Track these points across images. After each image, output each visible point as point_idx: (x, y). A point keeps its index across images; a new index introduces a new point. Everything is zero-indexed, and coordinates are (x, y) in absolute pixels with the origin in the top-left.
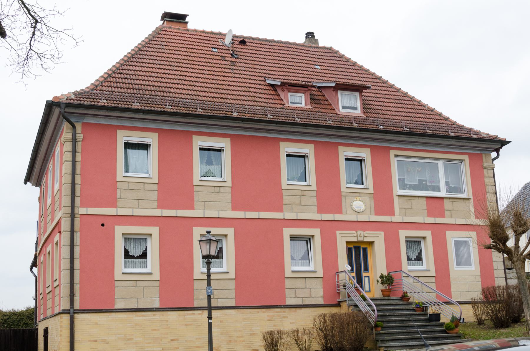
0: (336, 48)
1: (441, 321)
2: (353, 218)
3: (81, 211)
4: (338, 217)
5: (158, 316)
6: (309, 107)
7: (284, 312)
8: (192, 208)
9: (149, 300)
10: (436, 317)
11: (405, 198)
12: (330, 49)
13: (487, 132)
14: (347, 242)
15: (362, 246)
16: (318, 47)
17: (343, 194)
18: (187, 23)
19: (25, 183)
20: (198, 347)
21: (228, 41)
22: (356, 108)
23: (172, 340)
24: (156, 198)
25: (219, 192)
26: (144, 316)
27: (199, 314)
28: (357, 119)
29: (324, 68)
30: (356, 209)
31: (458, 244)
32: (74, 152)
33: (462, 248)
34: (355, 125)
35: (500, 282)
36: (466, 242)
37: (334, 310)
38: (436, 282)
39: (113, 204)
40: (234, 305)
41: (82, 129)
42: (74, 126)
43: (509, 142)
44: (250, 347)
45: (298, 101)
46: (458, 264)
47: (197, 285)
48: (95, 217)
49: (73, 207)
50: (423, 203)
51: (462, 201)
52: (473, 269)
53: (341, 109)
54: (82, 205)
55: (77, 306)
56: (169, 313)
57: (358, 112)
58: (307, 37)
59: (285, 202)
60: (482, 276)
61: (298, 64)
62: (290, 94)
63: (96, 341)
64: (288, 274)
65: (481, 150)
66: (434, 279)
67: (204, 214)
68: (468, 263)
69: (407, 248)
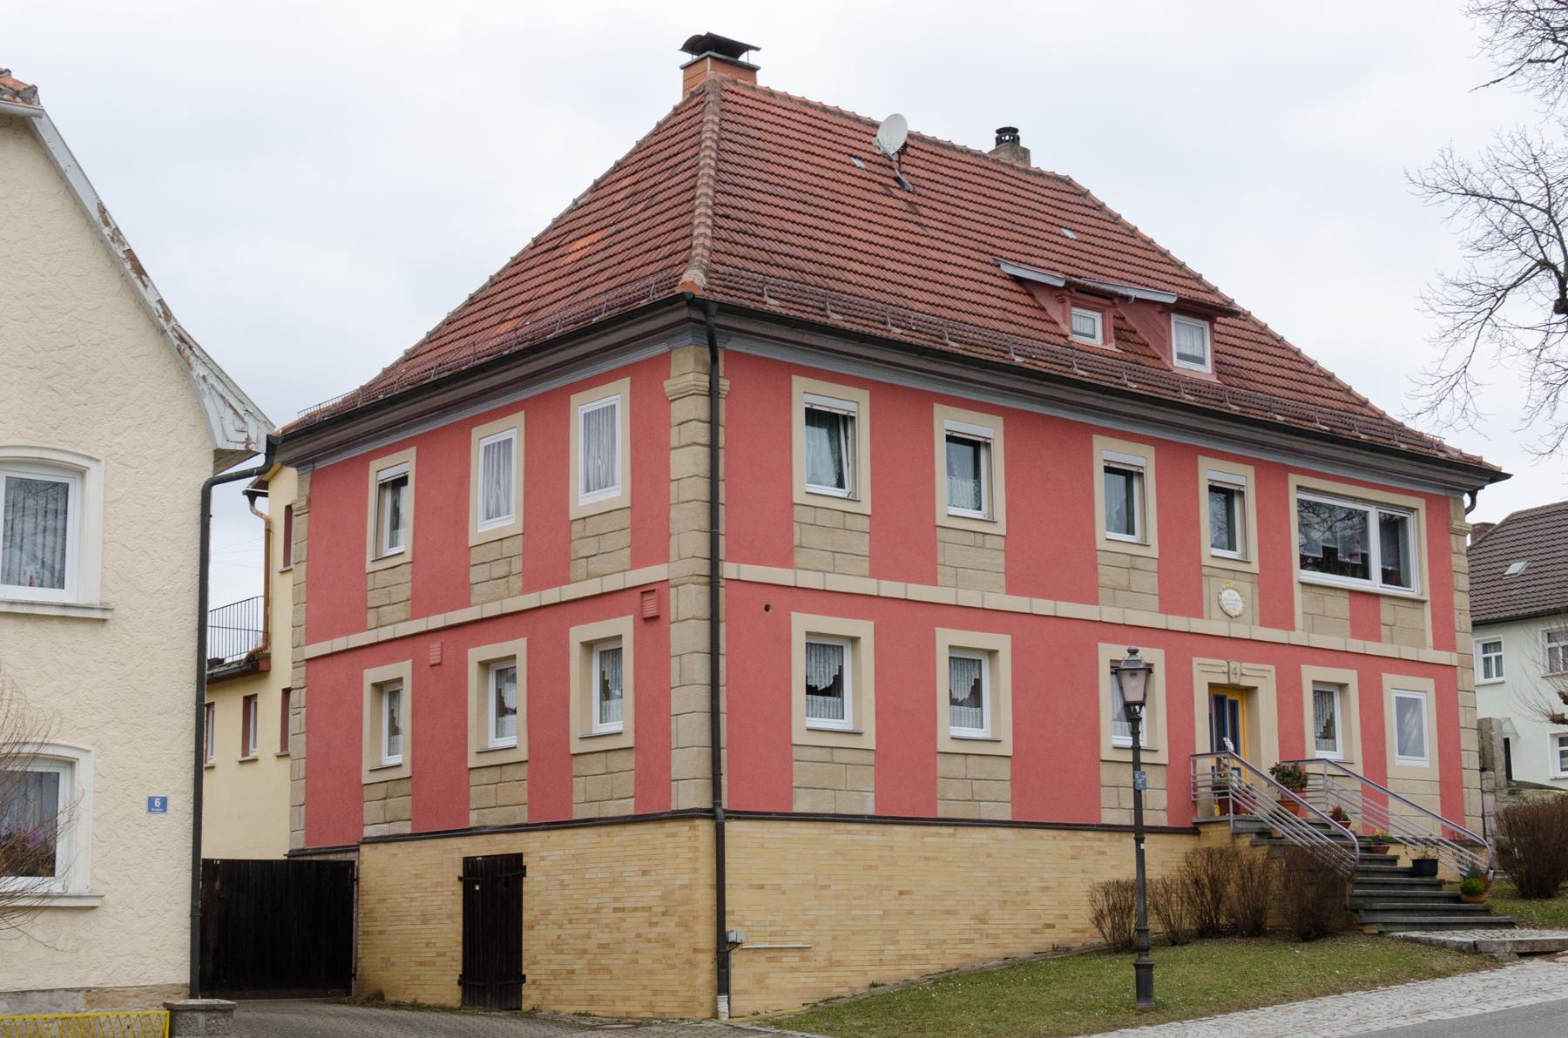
0: (1082, 181)
1: (1440, 876)
3: (729, 570)
4: (1197, 625)
5: (874, 836)
6: (1112, 347)
7: (1100, 840)
8: (932, 580)
9: (855, 796)
10: (1425, 867)
11: (1314, 590)
12: (1068, 182)
13: (1457, 447)
14: (1212, 686)
15: (1230, 697)
16: (1027, 171)
17: (1205, 571)
20: (948, 913)
22: (1201, 361)
23: (901, 893)
25: (983, 547)
26: (849, 832)
27: (950, 835)
28: (1196, 386)
29: (1085, 238)
30: (1227, 608)
32: (713, 423)
33: (1409, 716)
34: (1189, 399)
36: (1416, 702)
40: (1008, 818)
41: (1257, 478)
42: (714, 359)
43: (1507, 476)
44: (1039, 917)
45: (1088, 328)
46: (1402, 752)
47: (1107, 774)
50: (1342, 605)
51: (1410, 604)
52: (1427, 765)
53: (1177, 362)
54: (733, 558)
56: (896, 828)
57: (1206, 371)
58: (999, 141)
62: (1075, 310)
63: (762, 887)
64: (943, 744)
69: (808, 659)
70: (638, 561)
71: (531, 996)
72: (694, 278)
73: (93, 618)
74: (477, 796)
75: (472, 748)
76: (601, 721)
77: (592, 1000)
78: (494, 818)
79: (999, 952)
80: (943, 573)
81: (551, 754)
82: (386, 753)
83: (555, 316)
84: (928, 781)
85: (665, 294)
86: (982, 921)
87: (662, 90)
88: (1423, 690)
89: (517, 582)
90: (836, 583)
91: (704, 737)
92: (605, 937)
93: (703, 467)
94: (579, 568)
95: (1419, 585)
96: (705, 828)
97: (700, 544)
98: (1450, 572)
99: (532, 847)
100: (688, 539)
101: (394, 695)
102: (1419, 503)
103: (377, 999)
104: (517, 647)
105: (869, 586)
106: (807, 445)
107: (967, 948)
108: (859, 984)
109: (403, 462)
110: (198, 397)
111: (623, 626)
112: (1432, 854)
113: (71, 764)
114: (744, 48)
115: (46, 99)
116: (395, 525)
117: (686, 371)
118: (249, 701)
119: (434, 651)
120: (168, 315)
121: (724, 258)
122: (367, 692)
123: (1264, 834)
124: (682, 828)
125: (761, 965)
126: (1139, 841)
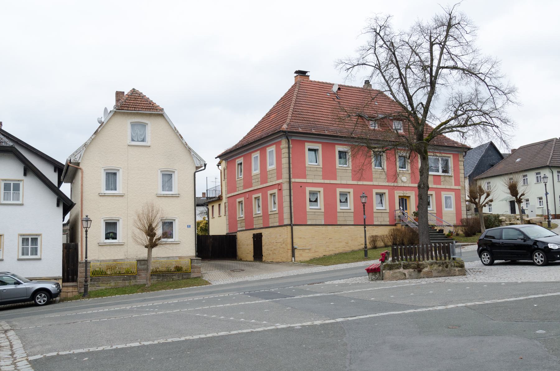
2: (402, 185)
3: (293, 180)
8: (336, 179)
10: (441, 231)
14: (399, 196)
18: (308, 76)
19: (216, 158)
21: (335, 89)
24: (321, 174)
31: (446, 198)
32: (289, 153)
35: (464, 216)
36: (450, 197)
37: (394, 227)
39: (305, 177)
42: (289, 141)
49: (290, 178)
54: (294, 178)
55: (293, 223)
58: (365, 83)
59: (374, 177)
60: (456, 214)
68: (450, 207)
70: (278, 179)
71: (264, 259)
72: (285, 127)
73: (177, 196)
74: (255, 222)
75: (254, 214)
76: (273, 208)
77: (273, 259)
78: (258, 226)
79: (351, 249)
80: (338, 178)
81: (266, 215)
82: (241, 215)
83: (264, 134)
84: (336, 217)
85: (279, 130)
86: (347, 243)
87: (290, 81)
88: (452, 195)
89: (259, 183)
90: (315, 181)
91: (289, 211)
92: (275, 248)
93: (287, 162)
94: (269, 180)
95: (451, 173)
96: (289, 227)
97: (287, 176)
98: (459, 169)
99: (263, 231)
100: (285, 175)
101: (258, 200)
102: (451, 156)
103: (241, 260)
104: (260, 195)
105: (322, 181)
106: (309, 156)
107: (344, 249)
108: (321, 255)
109: (241, 160)
110: (192, 158)
111: (275, 191)
112: (442, 228)
113: (175, 220)
114: (306, 72)
115: (165, 110)
116: (241, 172)
117: (284, 144)
118: (219, 205)
119: (247, 196)
120: (187, 144)
121: (294, 121)
122: (237, 203)
123: (407, 225)
124: (285, 228)
125: (301, 252)
126: (365, 228)
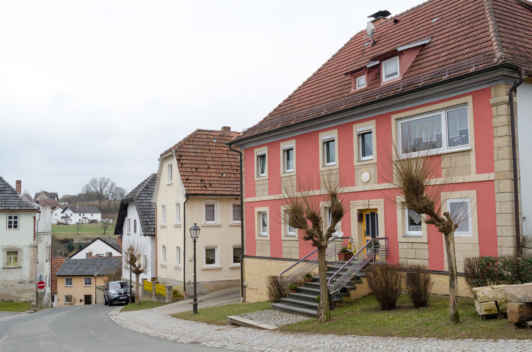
38: (429, 249)
48: (470, 184)
51: (462, 154)
61: (396, 39)
65: (488, 83)
66: (427, 245)
67: (489, 178)
